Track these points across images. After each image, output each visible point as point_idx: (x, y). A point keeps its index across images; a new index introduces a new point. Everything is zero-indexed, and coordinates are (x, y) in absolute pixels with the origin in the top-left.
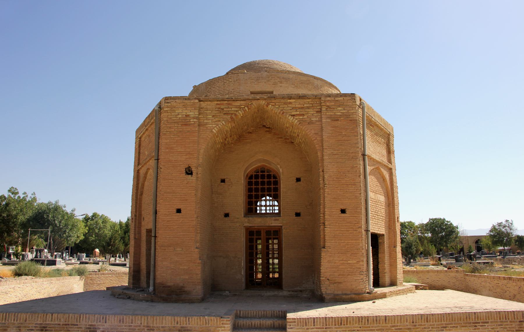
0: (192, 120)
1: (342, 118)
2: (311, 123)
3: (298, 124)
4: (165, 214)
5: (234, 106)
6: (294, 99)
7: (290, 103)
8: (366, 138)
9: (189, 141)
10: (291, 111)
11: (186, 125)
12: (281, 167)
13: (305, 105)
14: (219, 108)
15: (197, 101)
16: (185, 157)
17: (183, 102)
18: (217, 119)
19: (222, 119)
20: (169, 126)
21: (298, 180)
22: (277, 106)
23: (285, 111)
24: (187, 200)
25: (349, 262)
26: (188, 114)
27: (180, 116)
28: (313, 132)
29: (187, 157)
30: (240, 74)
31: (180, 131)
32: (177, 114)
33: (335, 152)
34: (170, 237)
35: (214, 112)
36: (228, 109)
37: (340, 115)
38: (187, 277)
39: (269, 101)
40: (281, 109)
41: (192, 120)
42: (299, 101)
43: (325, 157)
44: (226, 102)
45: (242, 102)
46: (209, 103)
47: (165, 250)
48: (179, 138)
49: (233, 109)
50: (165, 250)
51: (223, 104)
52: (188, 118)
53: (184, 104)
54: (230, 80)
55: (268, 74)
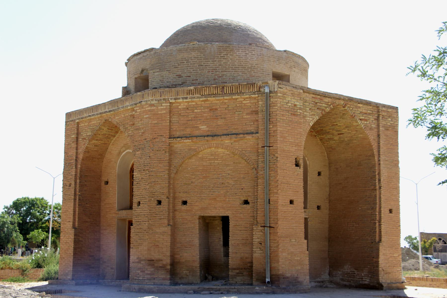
0: (298, 111)
1: (390, 129)
2: (371, 129)
3: (364, 128)
4: (282, 205)
5: (324, 102)
6: (362, 104)
7: (359, 107)
8: (376, 144)
9: (297, 132)
10: (359, 115)
11: (294, 115)
12: (308, 160)
13: (369, 112)
14: (314, 102)
15: (302, 91)
16: (294, 148)
17: (292, 91)
18: (313, 113)
19: (316, 113)
20: (282, 113)
21: (319, 174)
22: (351, 109)
23: (356, 114)
24: (298, 192)
25: (394, 255)
26: (296, 103)
27: (290, 104)
28: (373, 138)
29: (296, 148)
30: (263, 49)
31: (291, 121)
32: (287, 101)
33: (387, 159)
34: (286, 228)
35: (311, 105)
36: (321, 104)
37: (389, 126)
38: (300, 268)
39: (347, 103)
40: (353, 111)
41: (298, 111)
42: (365, 106)
43: (381, 163)
44: (319, 97)
45: (330, 99)
46: (308, 94)
47: (284, 240)
48: (290, 128)
49: (324, 105)
50: (284, 240)
51: (316, 98)
52: (296, 108)
53: (292, 92)
54: (253, 53)
55: (286, 55)
